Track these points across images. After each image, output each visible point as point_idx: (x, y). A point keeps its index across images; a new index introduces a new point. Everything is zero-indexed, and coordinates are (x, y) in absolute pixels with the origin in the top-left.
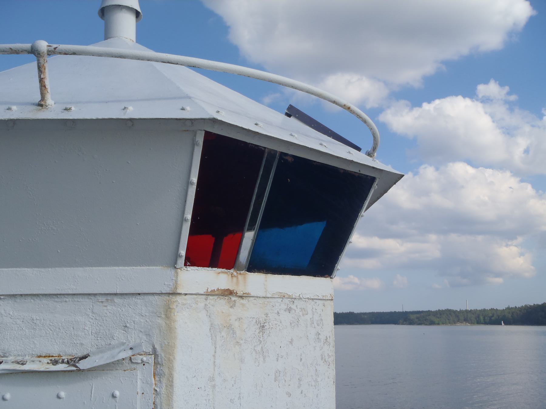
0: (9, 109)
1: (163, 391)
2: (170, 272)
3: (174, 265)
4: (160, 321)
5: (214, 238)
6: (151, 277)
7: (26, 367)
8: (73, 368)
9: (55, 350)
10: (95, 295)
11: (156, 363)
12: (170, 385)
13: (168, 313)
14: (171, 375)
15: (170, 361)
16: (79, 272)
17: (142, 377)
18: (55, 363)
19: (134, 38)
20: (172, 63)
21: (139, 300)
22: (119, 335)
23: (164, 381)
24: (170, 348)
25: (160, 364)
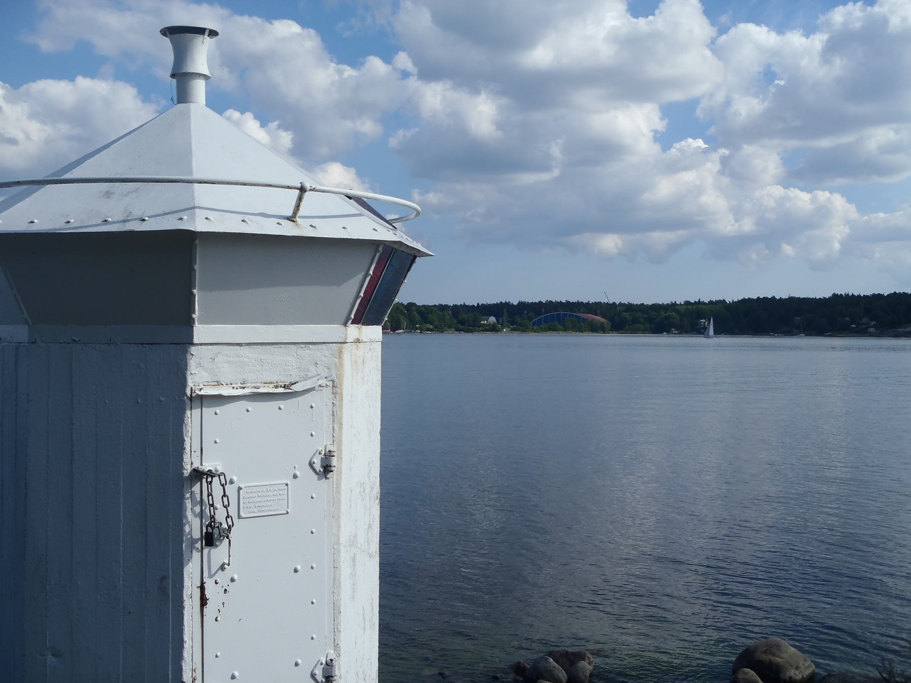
0: (181, 219)
1: (337, 403)
2: (342, 327)
3: (345, 324)
4: (336, 360)
5: (483, 96)
6: (330, 331)
7: (261, 390)
8: (287, 393)
9: (274, 379)
10: (298, 343)
11: (334, 386)
12: (341, 400)
13: (340, 353)
14: (342, 394)
15: (341, 385)
16: (290, 328)
17: (328, 392)
18: (276, 387)
19: (773, 35)
20: (213, 183)
21: (324, 346)
22: (313, 370)
23: (338, 397)
24: (340, 376)
25: (335, 386)
